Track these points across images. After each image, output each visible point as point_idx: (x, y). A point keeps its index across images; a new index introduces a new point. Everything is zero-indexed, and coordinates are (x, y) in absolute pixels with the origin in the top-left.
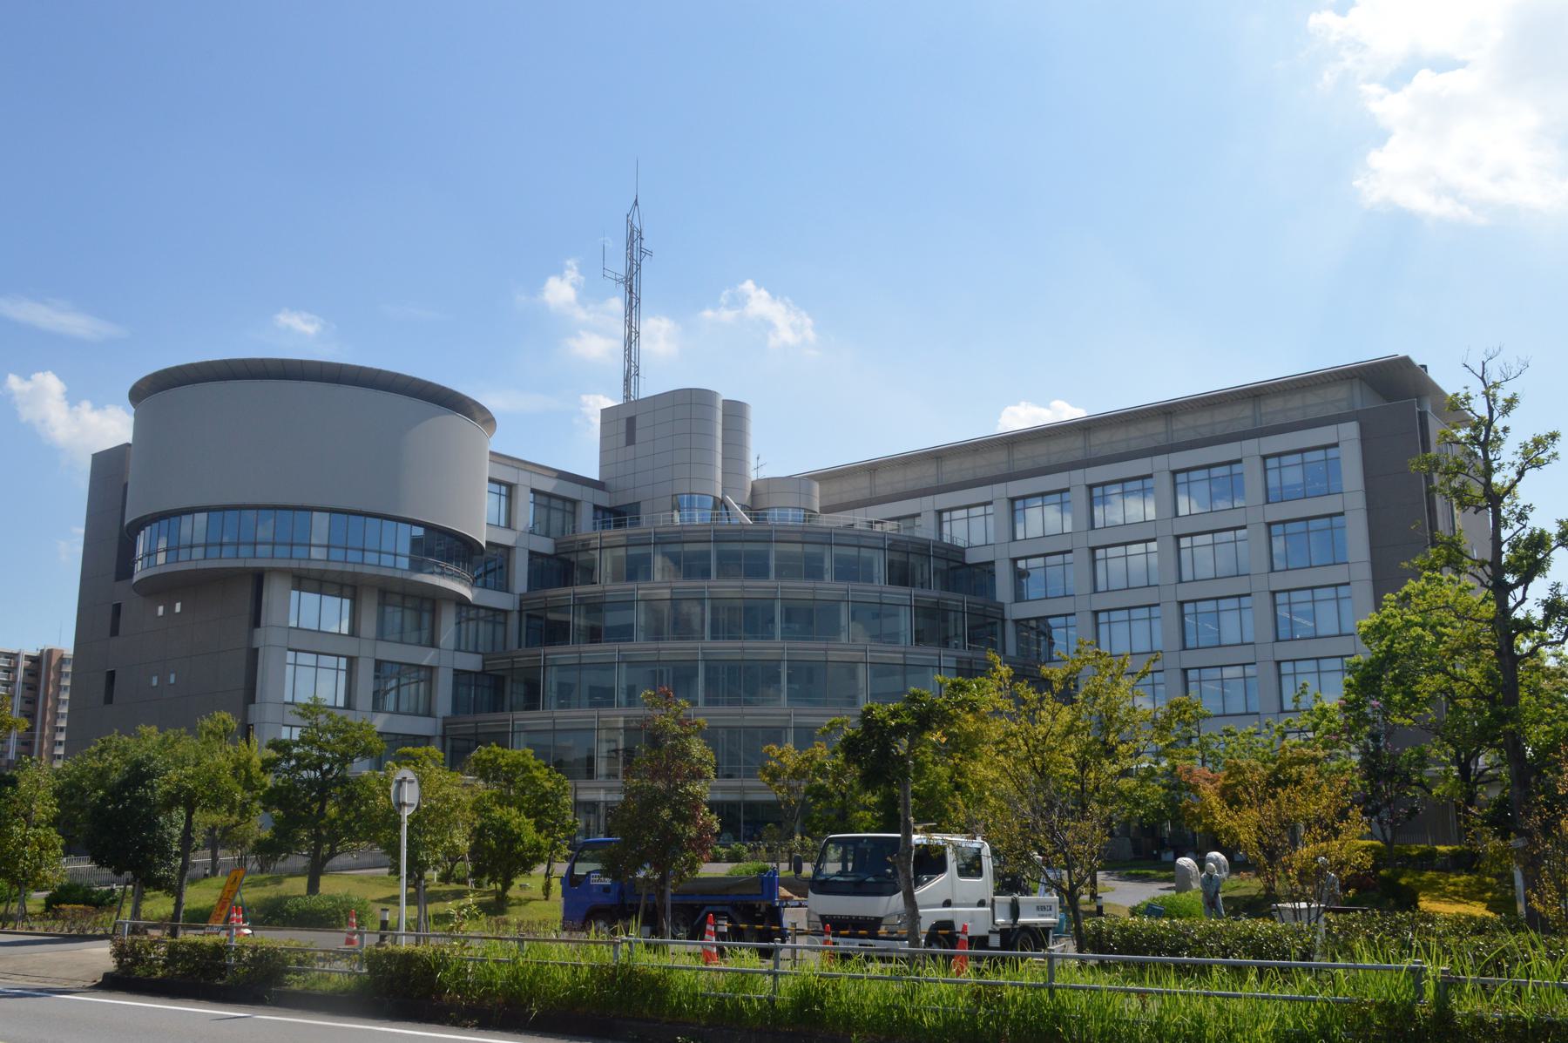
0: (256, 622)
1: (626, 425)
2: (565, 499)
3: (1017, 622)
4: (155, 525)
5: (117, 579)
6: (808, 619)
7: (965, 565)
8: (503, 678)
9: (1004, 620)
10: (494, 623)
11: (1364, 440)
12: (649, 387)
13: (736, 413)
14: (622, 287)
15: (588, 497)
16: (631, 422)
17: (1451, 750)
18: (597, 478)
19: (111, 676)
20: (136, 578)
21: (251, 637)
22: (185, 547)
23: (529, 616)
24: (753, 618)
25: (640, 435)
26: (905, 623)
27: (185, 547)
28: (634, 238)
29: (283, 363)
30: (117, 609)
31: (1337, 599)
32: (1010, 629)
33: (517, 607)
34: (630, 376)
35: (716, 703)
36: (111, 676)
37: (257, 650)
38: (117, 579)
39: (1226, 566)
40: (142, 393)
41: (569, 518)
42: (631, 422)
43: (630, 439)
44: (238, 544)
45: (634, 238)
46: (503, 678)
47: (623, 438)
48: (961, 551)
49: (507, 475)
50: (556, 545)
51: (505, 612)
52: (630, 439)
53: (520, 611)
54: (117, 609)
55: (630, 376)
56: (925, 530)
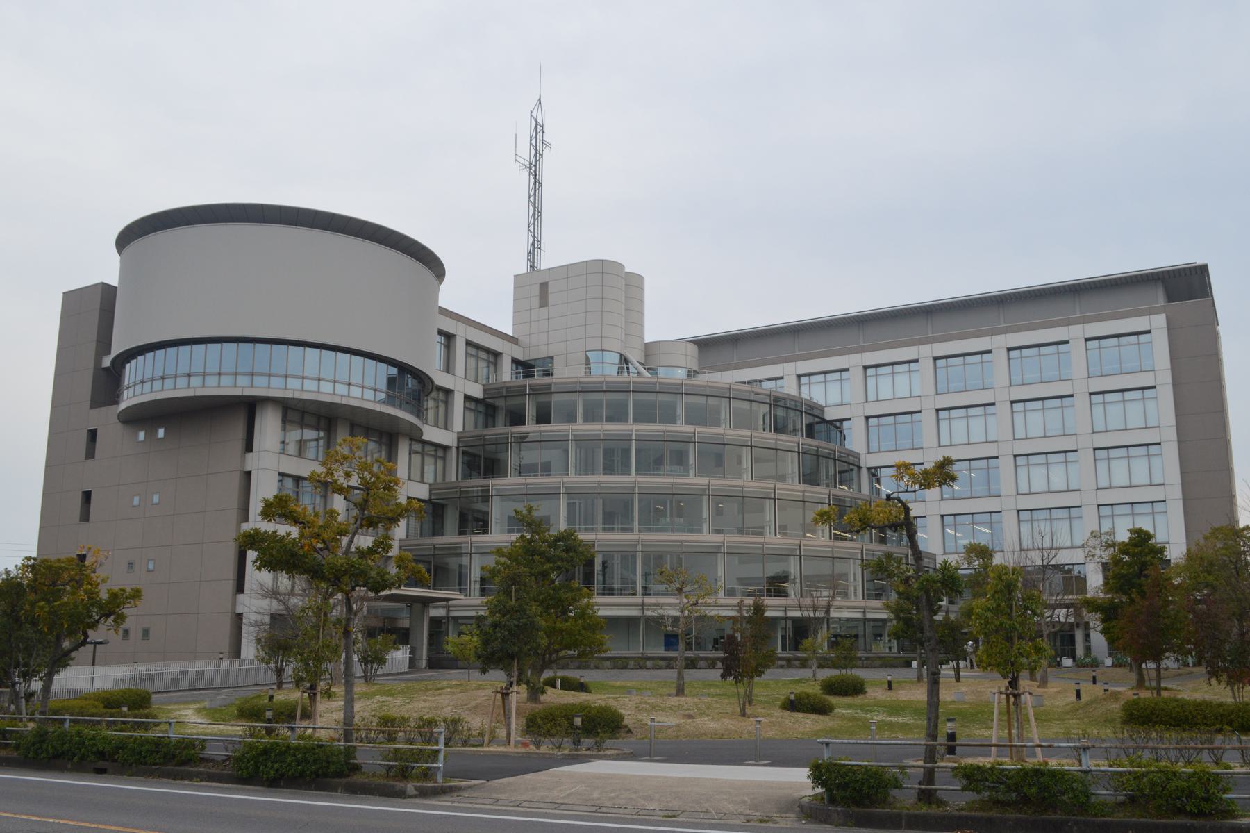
0: (249, 447)
1: (538, 289)
2: (488, 351)
3: (869, 469)
4: (141, 358)
5: (92, 407)
6: (717, 456)
7: (824, 421)
8: (443, 507)
9: (859, 468)
10: (436, 457)
11: (1170, 328)
12: (548, 261)
13: (634, 284)
14: (526, 172)
15: (509, 352)
16: (544, 287)
17: (1177, 581)
18: (511, 334)
19: (87, 496)
20: (123, 406)
21: (243, 461)
22: (183, 376)
23: (464, 453)
24: (657, 456)
25: (552, 299)
26: (792, 465)
27: (183, 376)
28: (538, 128)
29: (365, 224)
30: (93, 434)
31: (1047, 464)
32: (864, 473)
33: (455, 444)
34: (534, 248)
35: (611, 530)
36: (87, 496)
37: (249, 474)
38: (92, 407)
39: (977, 436)
40: (126, 238)
41: (492, 368)
42: (544, 287)
43: (544, 302)
44: (236, 374)
45: (538, 128)
46: (443, 507)
47: (536, 301)
48: (822, 409)
49: (450, 326)
50: (485, 391)
51: (446, 448)
52: (544, 302)
53: (458, 448)
54: (93, 434)
55: (534, 248)
56: (789, 388)
